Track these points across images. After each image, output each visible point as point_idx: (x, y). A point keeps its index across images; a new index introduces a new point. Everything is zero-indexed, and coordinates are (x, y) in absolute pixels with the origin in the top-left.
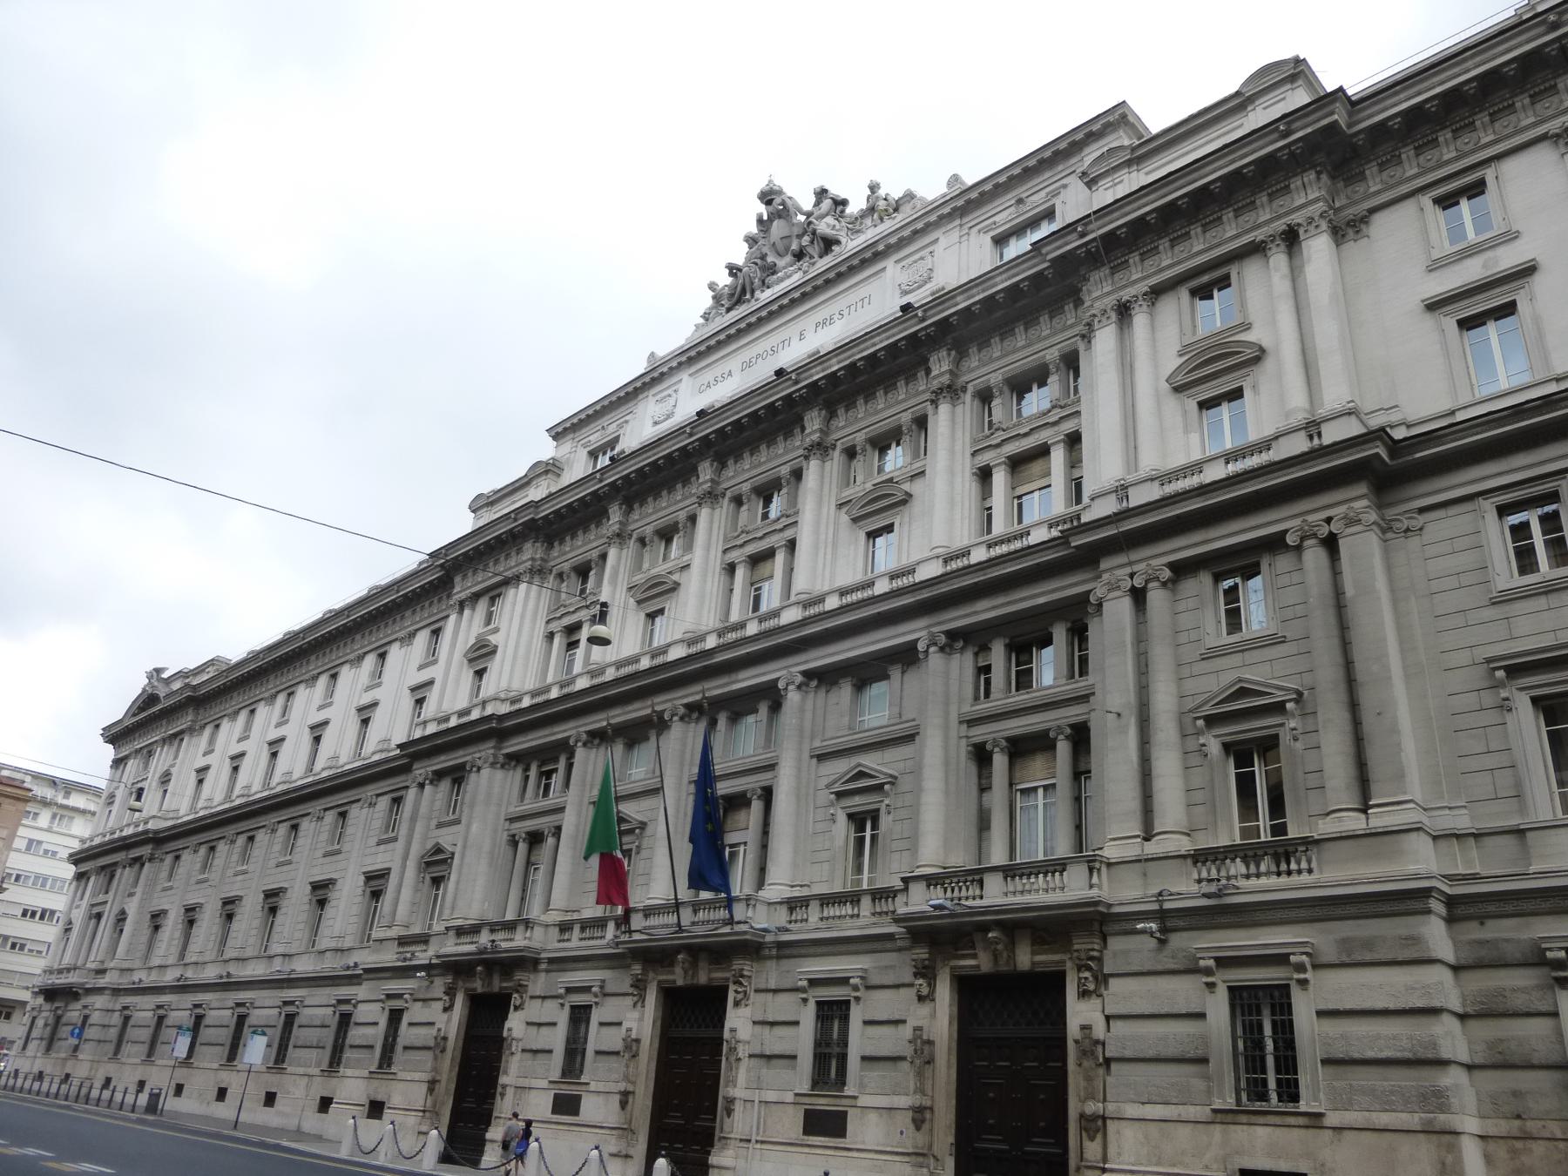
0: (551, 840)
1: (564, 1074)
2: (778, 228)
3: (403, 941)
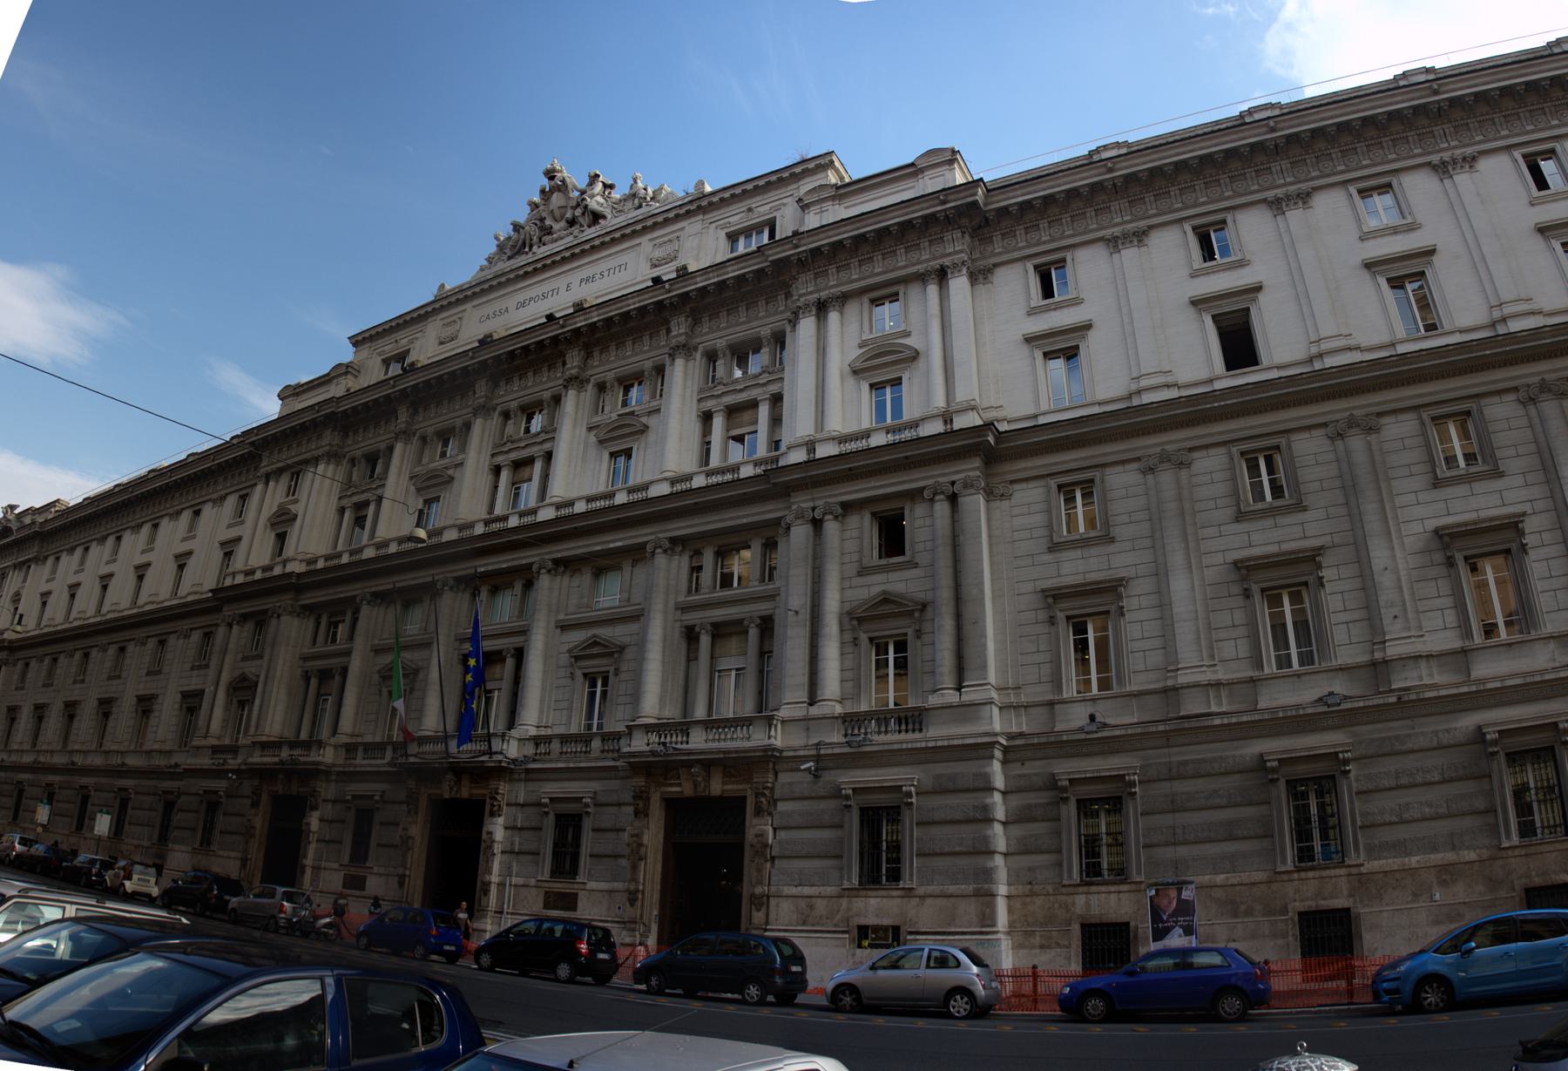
0: (337, 678)
1: (351, 860)
2: (557, 200)
3: (216, 750)
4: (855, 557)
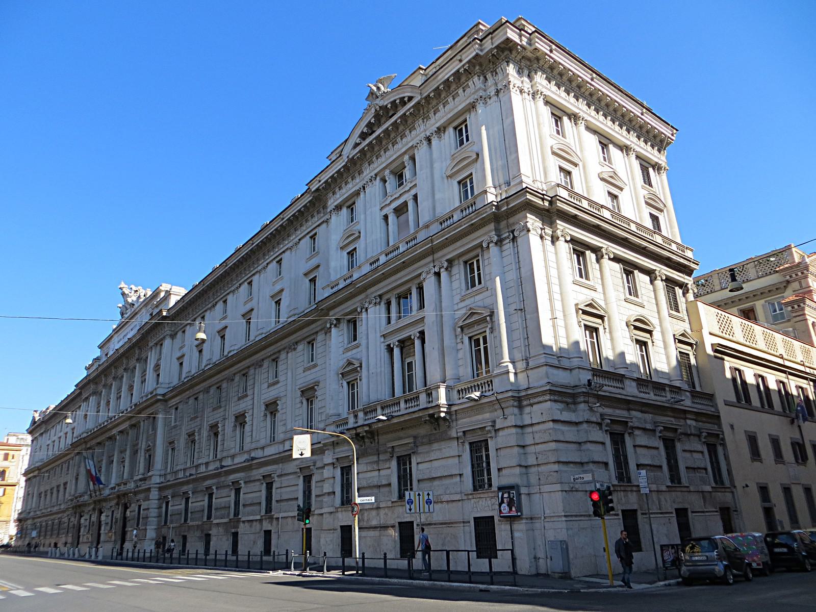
4: (454, 278)
